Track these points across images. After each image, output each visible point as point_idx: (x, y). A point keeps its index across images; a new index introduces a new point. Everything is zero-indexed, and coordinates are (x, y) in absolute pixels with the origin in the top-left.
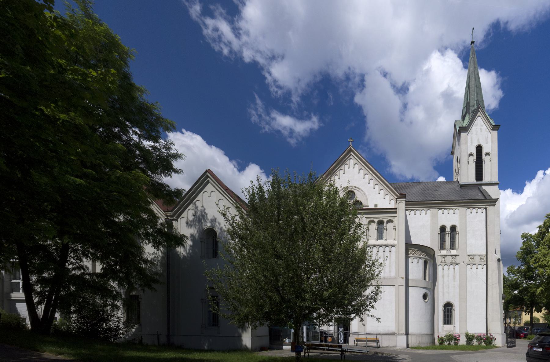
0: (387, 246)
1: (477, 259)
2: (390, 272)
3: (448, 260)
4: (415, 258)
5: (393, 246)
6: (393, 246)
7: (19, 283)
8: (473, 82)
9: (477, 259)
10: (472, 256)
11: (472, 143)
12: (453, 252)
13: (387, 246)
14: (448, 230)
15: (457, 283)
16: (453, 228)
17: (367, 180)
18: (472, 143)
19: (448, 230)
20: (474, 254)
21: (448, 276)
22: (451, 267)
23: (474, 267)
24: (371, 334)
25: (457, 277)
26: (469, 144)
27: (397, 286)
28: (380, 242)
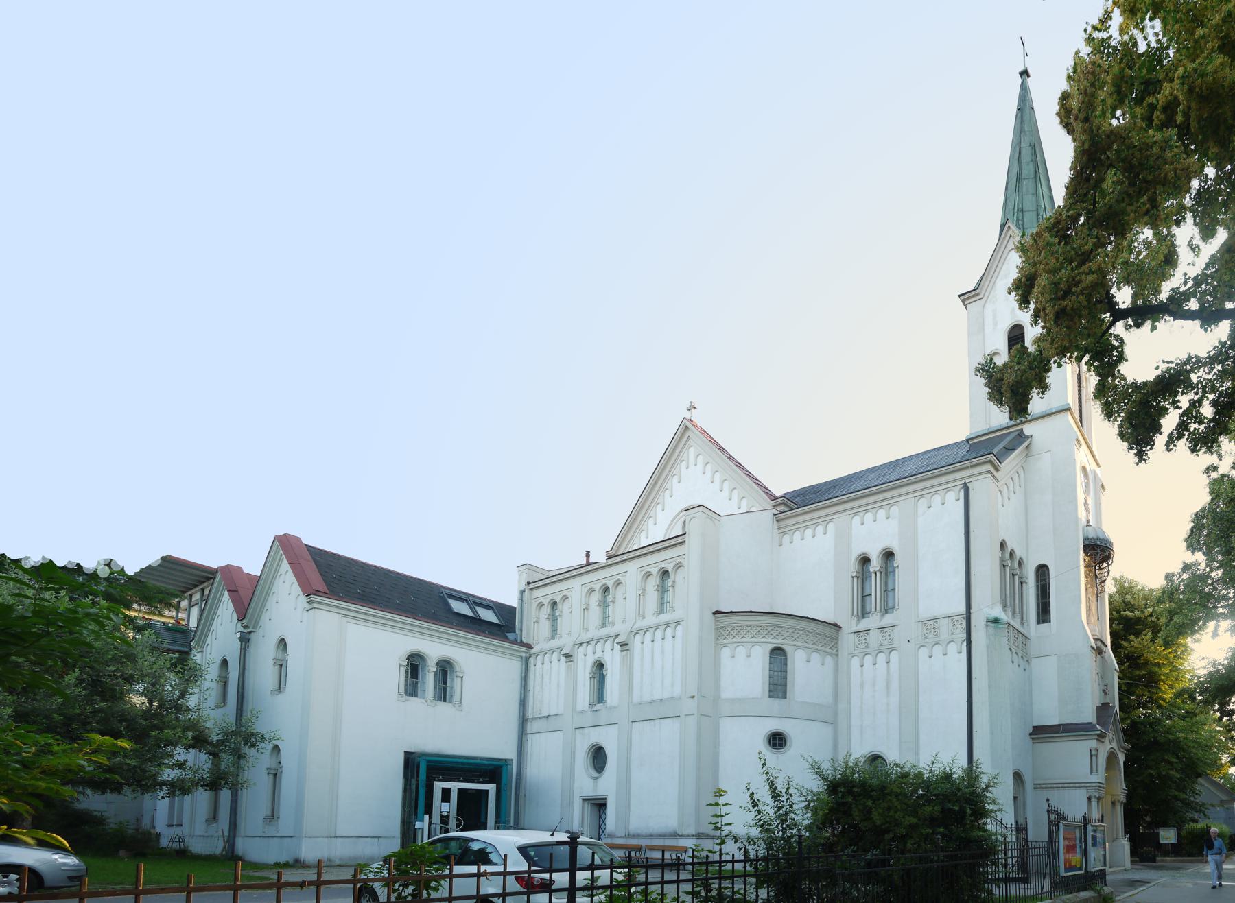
0: (667, 625)
1: (945, 625)
2: (672, 685)
3: (873, 637)
4: (740, 644)
5: (678, 623)
6: (678, 623)
7: (460, 791)
8: (1028, 170)
9: (945, 625)
10: (930, 624)
11: (995, 324)
12: (888, 619)
13: (667, 625)
14: (875, 564)
15: (894, 699)
16: (888, 555)
17: (717, 485)
18: (995, 324)
19: (875, 564)
20: (937, 613)
21: (874, 685)
22: (882, 658)
23: (938, 650)
24: (638, 836)
25: (895, 684)
26: (988, 328)
27: (682, 716)
28: (664, 618)
